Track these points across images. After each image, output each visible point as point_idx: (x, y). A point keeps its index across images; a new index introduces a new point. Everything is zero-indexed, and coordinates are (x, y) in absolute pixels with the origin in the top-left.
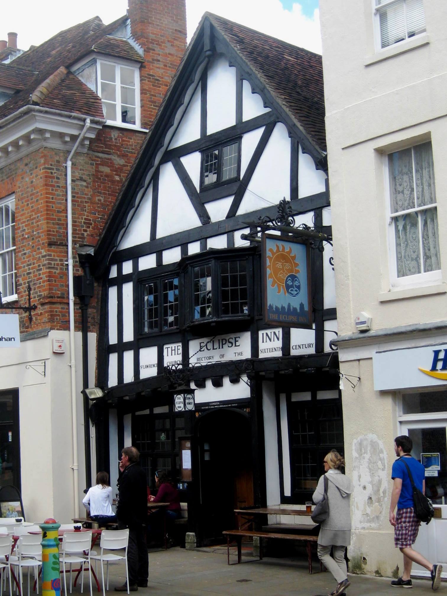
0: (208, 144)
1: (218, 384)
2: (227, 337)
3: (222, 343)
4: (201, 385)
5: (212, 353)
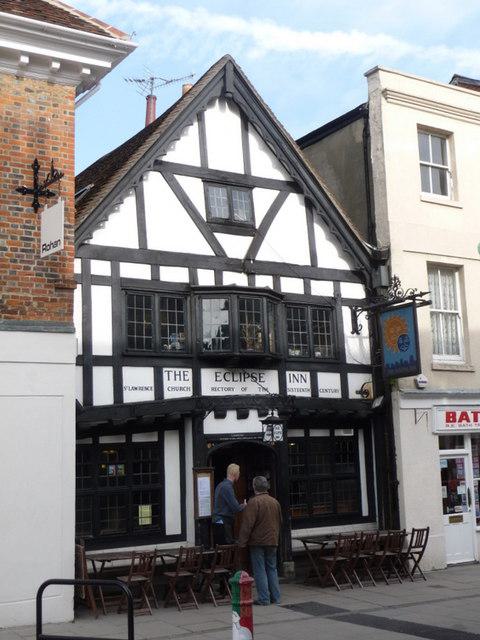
0: (213, 177)
1: (243, 415)
2: (250, 371)
3: (244, 376)
4: (220, 415)
5: (231, 384)
